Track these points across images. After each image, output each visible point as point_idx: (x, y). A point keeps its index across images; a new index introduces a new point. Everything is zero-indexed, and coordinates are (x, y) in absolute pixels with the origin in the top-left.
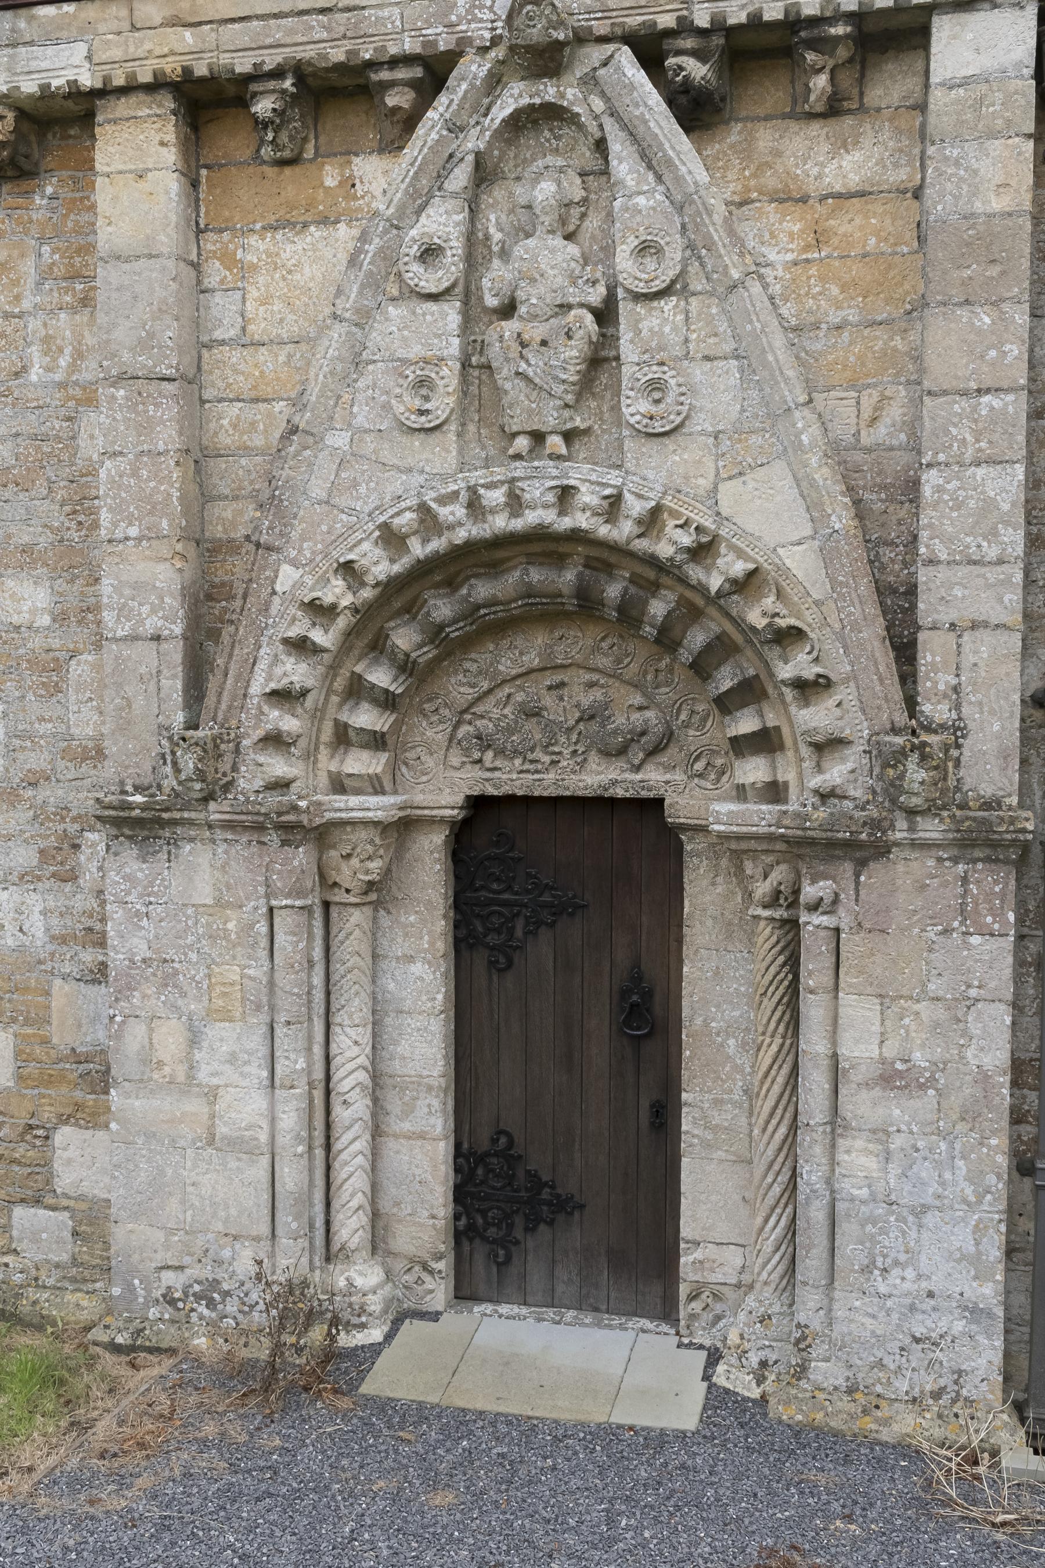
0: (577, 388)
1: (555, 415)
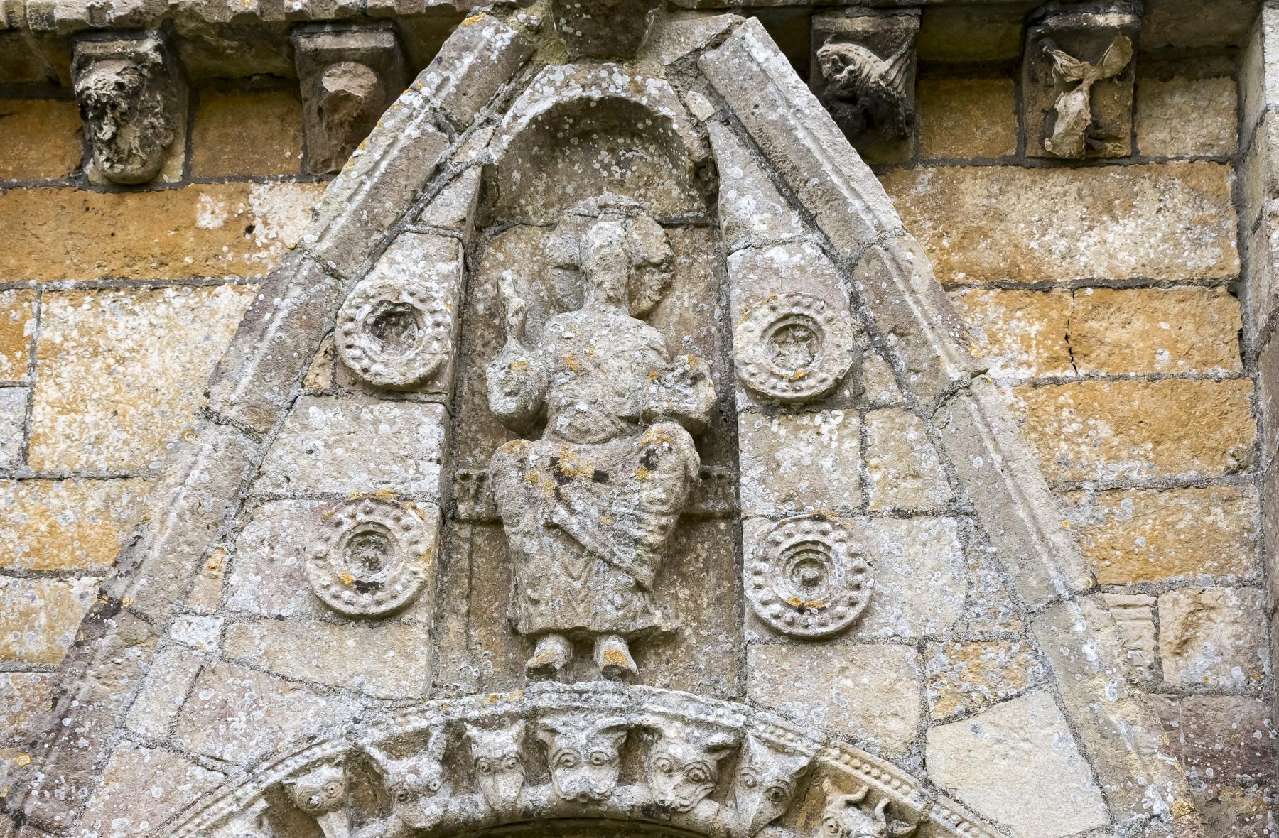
0: (658, 558)
1: (618, 600)
